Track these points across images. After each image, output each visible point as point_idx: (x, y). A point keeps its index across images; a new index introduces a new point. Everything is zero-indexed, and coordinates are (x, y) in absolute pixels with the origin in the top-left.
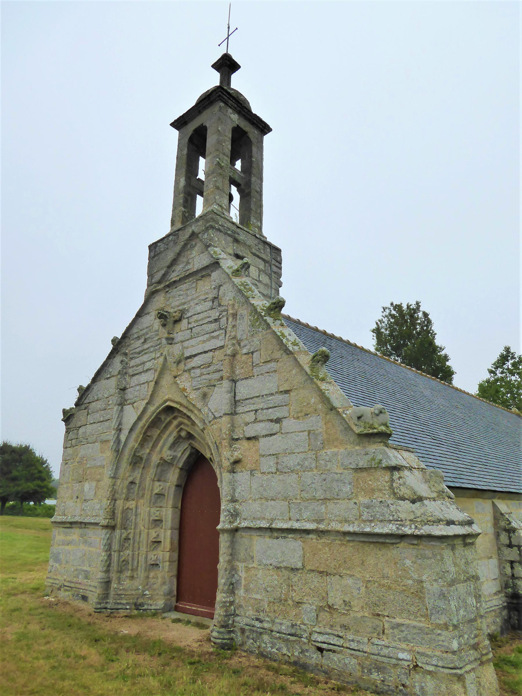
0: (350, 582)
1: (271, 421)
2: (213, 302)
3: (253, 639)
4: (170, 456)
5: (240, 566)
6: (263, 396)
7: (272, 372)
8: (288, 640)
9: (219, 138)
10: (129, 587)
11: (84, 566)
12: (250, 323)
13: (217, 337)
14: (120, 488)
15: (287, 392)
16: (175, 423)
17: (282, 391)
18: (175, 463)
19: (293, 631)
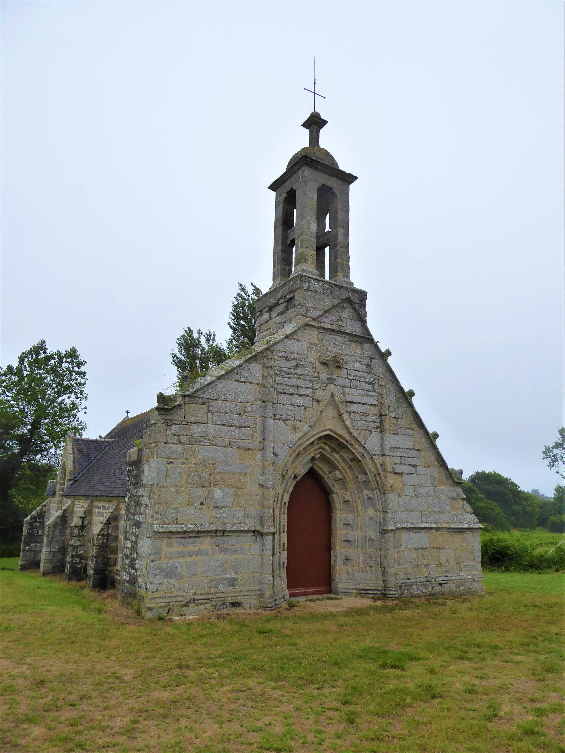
0: (448, 551)
1: (411, 465)
8: (426, 584)
9: (308, 197)
11: (226, 574)
13: (372, 396)
15: (419, 450)
19: (427, 580)
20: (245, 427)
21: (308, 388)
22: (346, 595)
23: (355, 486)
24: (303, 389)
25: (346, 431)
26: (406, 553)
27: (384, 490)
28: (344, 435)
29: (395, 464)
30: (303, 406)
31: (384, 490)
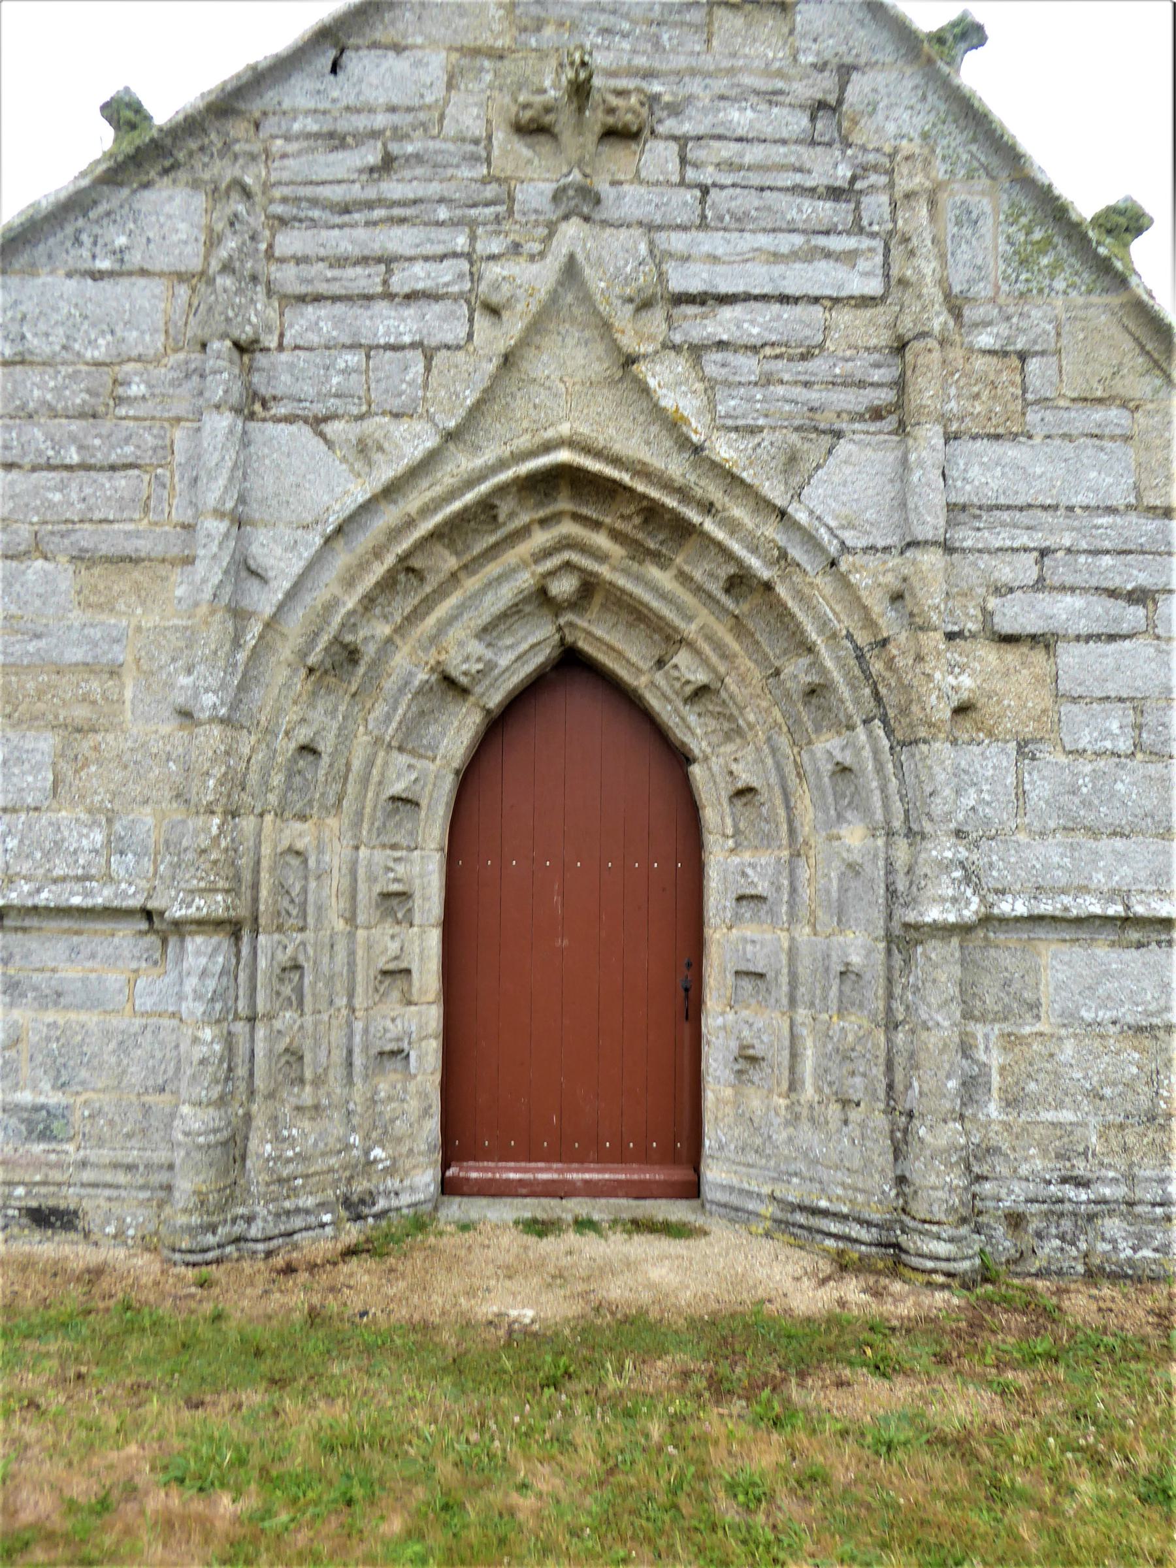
1: (1113, 593)
2: (813, 119)
3: (1062, 1238)
4: (479, 659)
5: (980, 1036)
6: (1070, 509)
7: (1113, 438)
10: (316, 1144)
11: (16, 1087)
12: (1010, 249)
13: (849, 257)
14: (254, 767)
16: (541, 538)
17: (1155, 508)
18: (478, 690)
20: (113, 468)
21: (443, 258)
22: (732, 1221)
23: (776, 713)
24: (418, 269)
25: (668, 444)
26: (1069, 1050)
27: (911, 725)
28: (657, 463)
30: (413, 345)
31: (911, 725)
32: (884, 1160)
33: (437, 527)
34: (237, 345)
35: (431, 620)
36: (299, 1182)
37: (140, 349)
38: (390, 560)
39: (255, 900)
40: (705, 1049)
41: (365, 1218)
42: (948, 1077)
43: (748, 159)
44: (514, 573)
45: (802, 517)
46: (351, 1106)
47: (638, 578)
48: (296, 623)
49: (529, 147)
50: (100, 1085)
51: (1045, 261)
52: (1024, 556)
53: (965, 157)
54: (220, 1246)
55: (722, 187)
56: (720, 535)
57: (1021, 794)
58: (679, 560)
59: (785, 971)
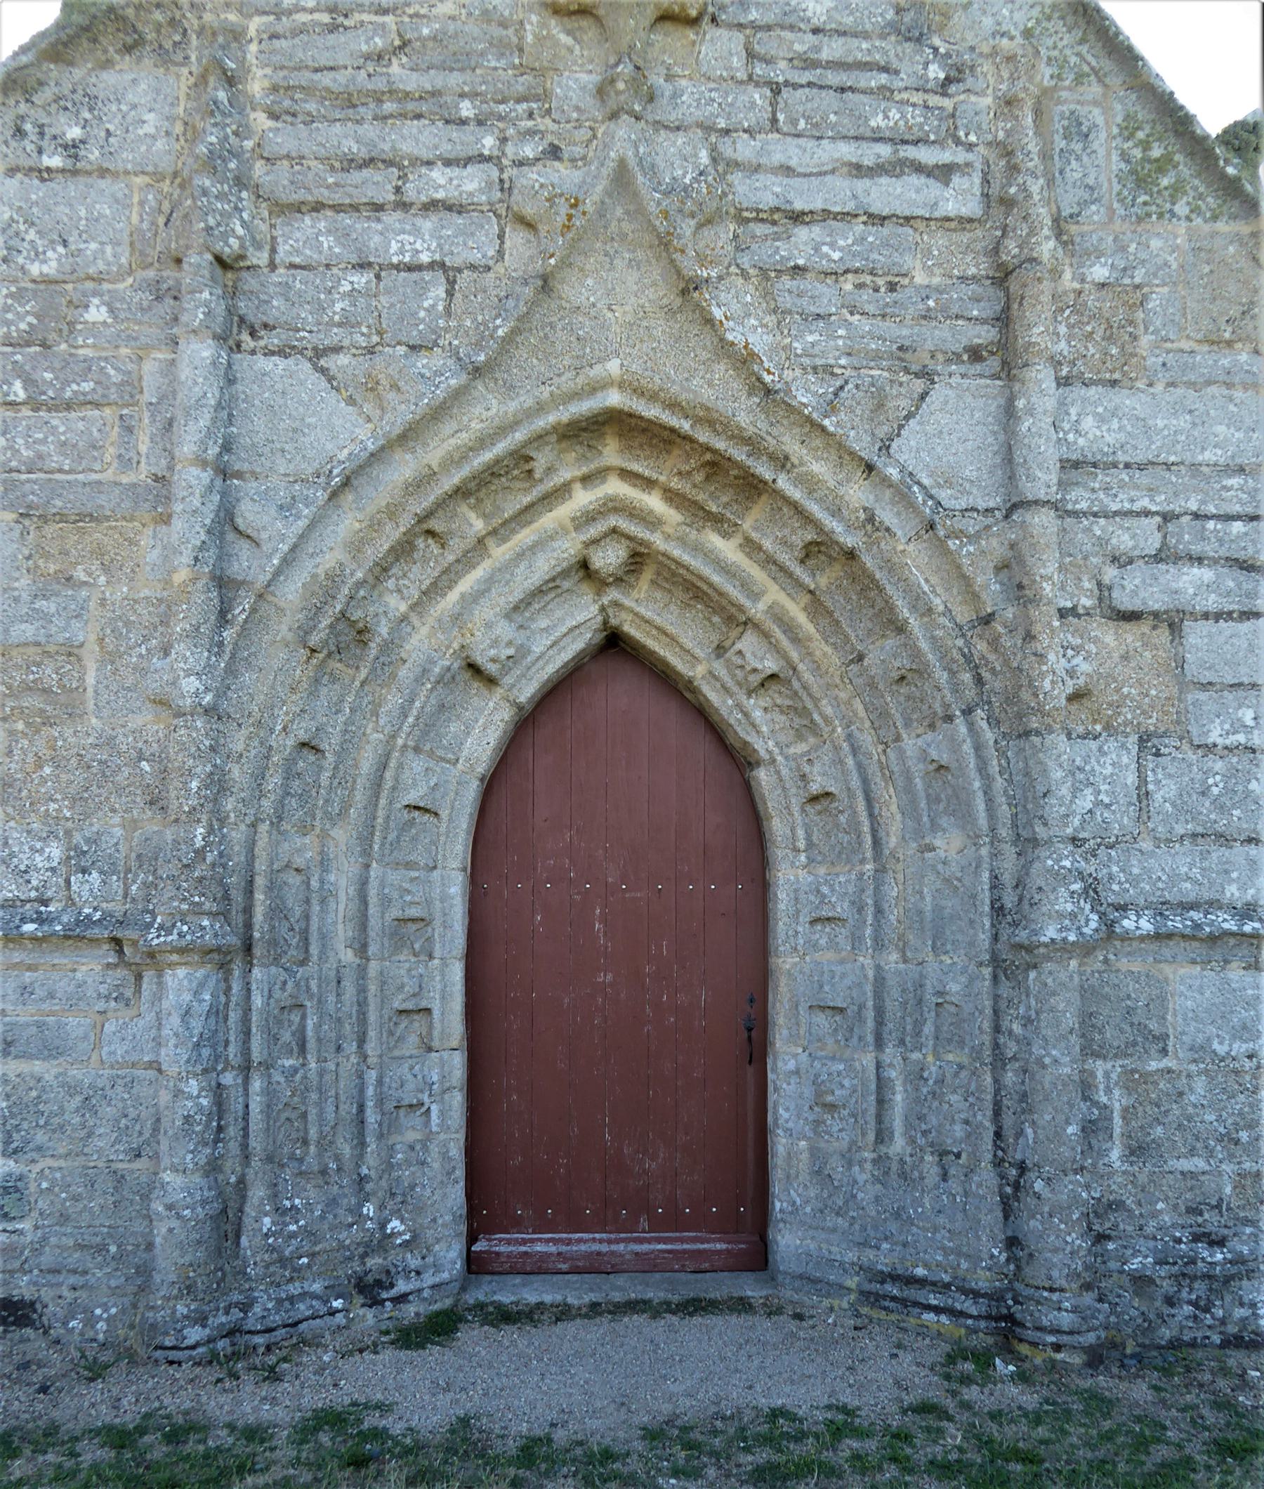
4: (509, 644)
5: (1100, 1074)
13: (944, 173)
16: (583, 498)
18: (508, 680)
21: (468, 161)
24: (438, 175)
28: (725, 407)
29: (1120, 561)
30: (432, 266)
32: (991, 1217)
33: (465, 481)
34: (219, 260)
35: (453, 596)
36: (305, 1260)
37: (101, 266)
38: (406, 521)
39: (248, 926)
40: (772, 1097)
41: (382, 1302)
42: (1068, 1123)
43: (825, 55)
44: (555, 535)
45: (893, 472)
46: (364, 1171)
47: (697, 549)
48: (292, 592)
49: (569, 33)
50: (62, 1151)
51: (1165, 182)
52: (1145, 521)
53: (1073, 60)
54: (210, 1340)
55: (796, 86)
56: (796, 494)
57: (1144, 795)
58: (747, 525)
59: (870, 1004)
